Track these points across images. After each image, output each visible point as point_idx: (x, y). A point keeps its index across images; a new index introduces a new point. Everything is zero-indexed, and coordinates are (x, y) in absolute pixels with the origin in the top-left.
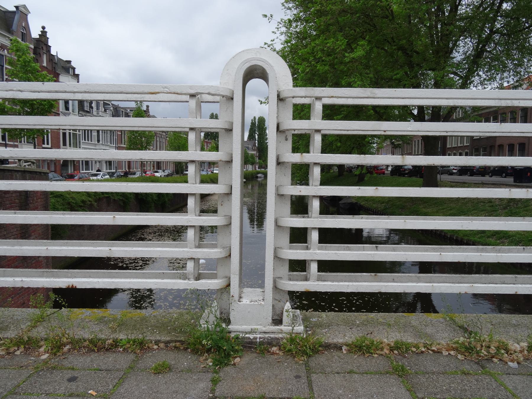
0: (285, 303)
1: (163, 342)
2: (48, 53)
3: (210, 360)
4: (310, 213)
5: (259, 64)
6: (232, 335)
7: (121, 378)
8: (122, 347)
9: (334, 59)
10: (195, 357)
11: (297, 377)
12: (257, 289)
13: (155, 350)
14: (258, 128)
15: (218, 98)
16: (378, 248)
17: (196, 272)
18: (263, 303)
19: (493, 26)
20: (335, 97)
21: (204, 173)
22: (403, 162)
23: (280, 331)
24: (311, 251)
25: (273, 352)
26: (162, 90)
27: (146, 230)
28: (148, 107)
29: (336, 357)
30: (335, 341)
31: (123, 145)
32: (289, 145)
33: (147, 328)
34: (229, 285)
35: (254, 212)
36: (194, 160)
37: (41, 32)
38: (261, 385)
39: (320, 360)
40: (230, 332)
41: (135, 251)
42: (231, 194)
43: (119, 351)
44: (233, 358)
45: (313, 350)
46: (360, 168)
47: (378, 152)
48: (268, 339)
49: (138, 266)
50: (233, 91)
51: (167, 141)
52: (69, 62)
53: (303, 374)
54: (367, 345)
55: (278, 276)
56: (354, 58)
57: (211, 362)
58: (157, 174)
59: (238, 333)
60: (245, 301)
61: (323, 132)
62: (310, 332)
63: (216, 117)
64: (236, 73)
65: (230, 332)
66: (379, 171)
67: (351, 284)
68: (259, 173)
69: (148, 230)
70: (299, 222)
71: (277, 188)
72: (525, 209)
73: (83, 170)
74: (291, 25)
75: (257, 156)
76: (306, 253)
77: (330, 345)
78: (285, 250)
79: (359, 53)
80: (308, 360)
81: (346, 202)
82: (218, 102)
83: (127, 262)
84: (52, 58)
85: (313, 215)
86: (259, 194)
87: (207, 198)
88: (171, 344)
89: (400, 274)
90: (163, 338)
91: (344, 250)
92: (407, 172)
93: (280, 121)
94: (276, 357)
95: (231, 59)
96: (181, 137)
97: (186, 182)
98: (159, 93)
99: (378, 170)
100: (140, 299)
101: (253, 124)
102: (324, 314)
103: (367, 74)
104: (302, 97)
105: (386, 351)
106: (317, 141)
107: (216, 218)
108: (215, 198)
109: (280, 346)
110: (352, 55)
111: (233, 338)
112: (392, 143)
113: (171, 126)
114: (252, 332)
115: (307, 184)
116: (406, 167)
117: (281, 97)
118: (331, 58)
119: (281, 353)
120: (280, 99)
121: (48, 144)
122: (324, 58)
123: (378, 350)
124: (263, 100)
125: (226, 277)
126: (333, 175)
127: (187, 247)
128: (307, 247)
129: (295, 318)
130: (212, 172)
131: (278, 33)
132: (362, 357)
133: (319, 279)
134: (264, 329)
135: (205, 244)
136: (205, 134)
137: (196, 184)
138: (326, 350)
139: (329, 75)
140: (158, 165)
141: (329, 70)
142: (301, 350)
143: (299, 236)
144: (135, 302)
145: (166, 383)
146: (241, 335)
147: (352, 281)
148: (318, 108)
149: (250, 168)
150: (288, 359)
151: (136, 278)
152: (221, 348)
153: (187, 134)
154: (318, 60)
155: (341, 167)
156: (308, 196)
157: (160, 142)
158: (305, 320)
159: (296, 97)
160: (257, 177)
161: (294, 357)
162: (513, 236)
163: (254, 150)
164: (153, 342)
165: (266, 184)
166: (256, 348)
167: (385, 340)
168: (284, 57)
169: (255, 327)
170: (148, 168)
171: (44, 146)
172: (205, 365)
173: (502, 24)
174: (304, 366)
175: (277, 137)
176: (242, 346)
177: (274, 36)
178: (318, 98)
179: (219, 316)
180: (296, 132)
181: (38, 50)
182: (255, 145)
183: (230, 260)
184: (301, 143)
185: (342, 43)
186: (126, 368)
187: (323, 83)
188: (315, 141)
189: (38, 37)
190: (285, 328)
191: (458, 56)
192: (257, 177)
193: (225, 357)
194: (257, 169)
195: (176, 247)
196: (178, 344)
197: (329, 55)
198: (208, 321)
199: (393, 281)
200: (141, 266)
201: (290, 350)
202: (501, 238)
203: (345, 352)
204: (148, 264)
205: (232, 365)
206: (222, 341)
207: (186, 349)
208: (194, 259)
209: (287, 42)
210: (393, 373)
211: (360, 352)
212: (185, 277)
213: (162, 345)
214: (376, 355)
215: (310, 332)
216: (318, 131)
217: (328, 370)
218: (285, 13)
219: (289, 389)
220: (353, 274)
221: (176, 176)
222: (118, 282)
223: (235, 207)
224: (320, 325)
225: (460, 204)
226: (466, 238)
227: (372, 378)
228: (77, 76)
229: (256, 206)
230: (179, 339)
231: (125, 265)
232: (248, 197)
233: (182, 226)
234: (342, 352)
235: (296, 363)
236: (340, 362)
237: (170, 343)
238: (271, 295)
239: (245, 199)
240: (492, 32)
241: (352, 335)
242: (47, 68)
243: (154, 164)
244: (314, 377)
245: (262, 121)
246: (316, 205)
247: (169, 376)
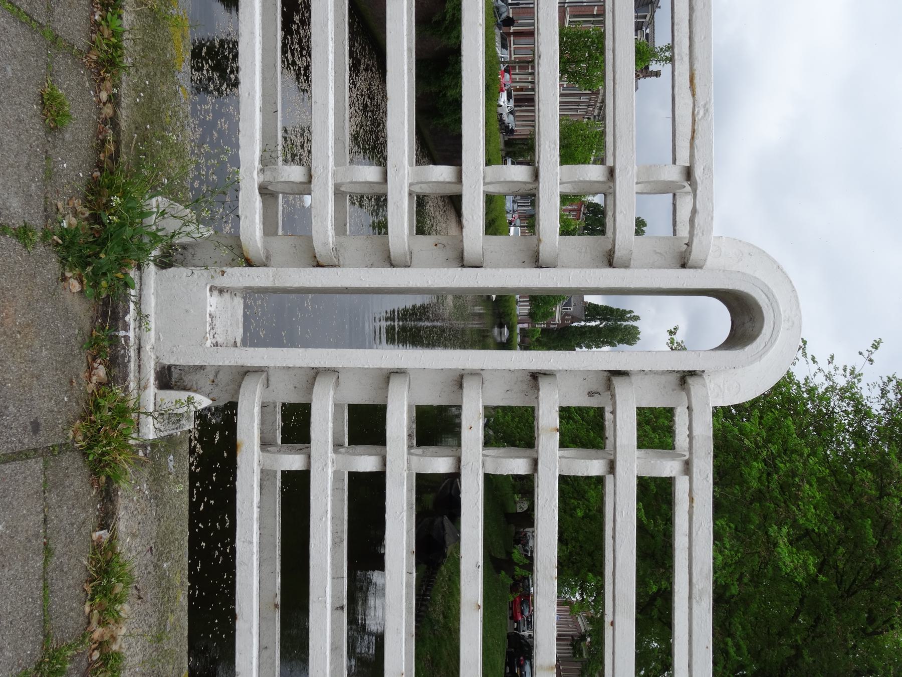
0: (208, 396)
1: (115, 112)
3: (74, 221)
4: (419, 451)
5: (765, 327)
6: (133, 273)
7: (32, 19)
8: (104, 18)
9: (773, 499)
10: (80, 187)
11: (36, 427)
12: (241, 330)
13: (97, 96)
14: (613, 327)
15: (683, 231)
16: (339, 612)
17: (279, 188)
18: (208, 343)
20: (691, 507)
21: (509, 205)
22: (542, 667)
23: (143, 383)
24: (331, 454)
25: (93, 368)
26: (701, 102)
27: (376, 76)
28: (657, 74)
29: (83, 516)
30: (122, 513)
31: (568, 19)
32: (578, 399)
33: (148, 76)
34: (249, 264)
35: (420, 320)
36: (541, 180)
38: (16, 342)
39: (77, 479)
40: (139, 267)
41: (327, 45)
42: (463, 266)
43: (93, 13)
44: (80, 275)
45: (100, 461)
46: (527, 561)
47: (562, 602)
48: (124, 356)
49: (293, 55)
50: (701, 268)
51: (580, 118)
53: (41, 440)
54: (113, 587)
55: (272, 379)
56: (776, 545)
57: (70, 224)
58: (504, 96)
59: (137, 286)
60: (213, 302)
61: (609, 479)
62: (141, 454)
63: (639, 232)
64: (744, 274)
65: (139, 267)
66: (518, 606)
67: (255, 549)
68: (511, 329)
69: (376, 82)
70: (399, 424)
71: (476, 374)
75: (548, 324)
76: (327, 442)
77: (112, 502)
78: (332, 392)
79: (787, 557)
80: (75, 449)
81: (448, 530)
82: (675, 234)
83: (302, 32)
85: (415, 459)
86: (463, 331)
87: (453, 210)
88: (110, 132)
89: (278, 662)
90: (124, 112)
91: (335, 532)
92: (517, 671)
93: (634, 378)
94: (83, 375)
95: (775, 262)
96: (591, 150)
97: (488, 163)
98: (693, 95)
99: (522, 603)
100: (217, 62)
101: (622, 314)
102: (183, 487)
103: (740, 579)
104: (690, 428)
105: (98, 632)
106: (590, 466)
107: (406, 231)
108: (453, 230)
109: (107, 384)
110: (783, 542)
111: (126, 274)
112: (583, 637)
113: (618, 123)
114: (141, 317)
115: (487, 443)
116: (527, 668)
117: (690, 380)
118: (776, 493)
119: (91, 387)
120: (685, 378)
122: (776, 476)
123: (100, 613)
124: (678, 338)
125: (267, 258)
126: (509, 504)
127: (337, 164)
128: (341, 446)
129: (173, 419)
130: (510, 223)
131: (831, 368)
132: (83, 576)
133: (266, 475)
134: (148, 347)
135: (345, 207)
136: (597, 204)
137: (485, 184)
138: (100, 493)
139: (737, 489)
140: (526, 100)
141: (748, 488)
142: (99, 436)
143: (366, 425)
144: (211, 49)
145: (20, 121)
146: (133, 292)
147: (261, 551)
148: (665, 467)
149: (522, 309)
150: (78, 403)
151: (264, 49)
152: (101, 249)
153: (601, 161)
154: (770, 463)
155: (528, 518)
156: (459, 445)
157: (577, 104)
158: (170, 442)
159: (690, 416)
160: (501, 326)
161: (83, 419)
163: (563, 319)
164: (115, 91)
165: (485, 347)
166: (103, 329)
167: (124, 631)
168: (777, 388)
169: (152, 325)
170: (517, 78)
172: (61, 210)
174: (61, 441)
175: (597, 372)
176: (108, 296)
177: (823, 363)
178: (687, 467)
179: (176, 241)
180: (608, 416)
182: (574, 319)
183: (309, 266)
184: (585, 428)
185: (809, 517)
186: (54, 29)
187: (723, 476)
188: (588, 462)
190: (151, 396)
192: (501, 326)
193: (81, 257)
194: (520, 326)
195: (337, 140)
196: (111, 147)
197: (783, 488)
198: (163, 214)
199: (262, 648)
200: (294, 63)
201: (98, 407)
203: (95, 536)
204: (298, 78)
205: (63, 274)
206: (118, 249)
207: (99, 166)
208: (310, 182)
209: (811, 391)
210: (47, 650)
211: (96, 572)
212: (267, 161)
213: (108, 110)
214: (87, 609)
215: (141, 454)
216: (612, 467)
217: (53, 498)
218: (874, 384)
219: (6, 408)
220: (278, 552)
221: (500, 139)
222: (253, 8)
223: (430, 276)
224: (158, 478)
227: (34, 601)
229: (436, 323)
230: (123, 149)
231: (294, 27)
232: (455, 307)
233: (385, 159)
234: (95, 531)
235: (70, 424)
236: (73, 524)
237: (114, 129)
238: (227, 363)
239: (450, 299)
241: (134, 553)
243: (527, 90)
244: (36, 465)
245: (629, 336)
246: (440, 465)
247: (36, 129)
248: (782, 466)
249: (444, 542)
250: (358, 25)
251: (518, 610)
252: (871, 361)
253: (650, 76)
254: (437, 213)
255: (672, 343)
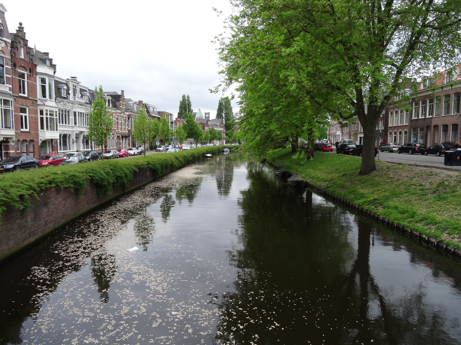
2: (25, 47)
19: (425, 19)
37: (19, 27)
52: (47, 54)
66: (327, 148)
68: (225, 147)
72: (453, 194)
73: (61, 150)
74: (238, 22)
84: (29, 51)
92: (351, 150)
121: (26, 128)
122: (264, 53)
124: (213, 89)
160: (223, 151)
162: (440, 223)
163: (222, 127)
170: (124, 146)
171: (22, 130)
173: (434, 17)
177: (222, 30)
181: (15, 44)
182: (222, 123)
185: (279, 39)
189: (16, 32)
191: (393, 48)
192: (223, 151)
194: (224, 143)
202: (429, 224)
225: (394, 186)
226: (396, 222)
228: (54, 67)
240: (424, 26)
242: (24, 60)
248: (259, 50)
249: (297, 181)
250: (81, 219)
251: (328, 148)
252: (221, 12)
253: (123, 94)
254: (169, 182)
255: (215, 92)
